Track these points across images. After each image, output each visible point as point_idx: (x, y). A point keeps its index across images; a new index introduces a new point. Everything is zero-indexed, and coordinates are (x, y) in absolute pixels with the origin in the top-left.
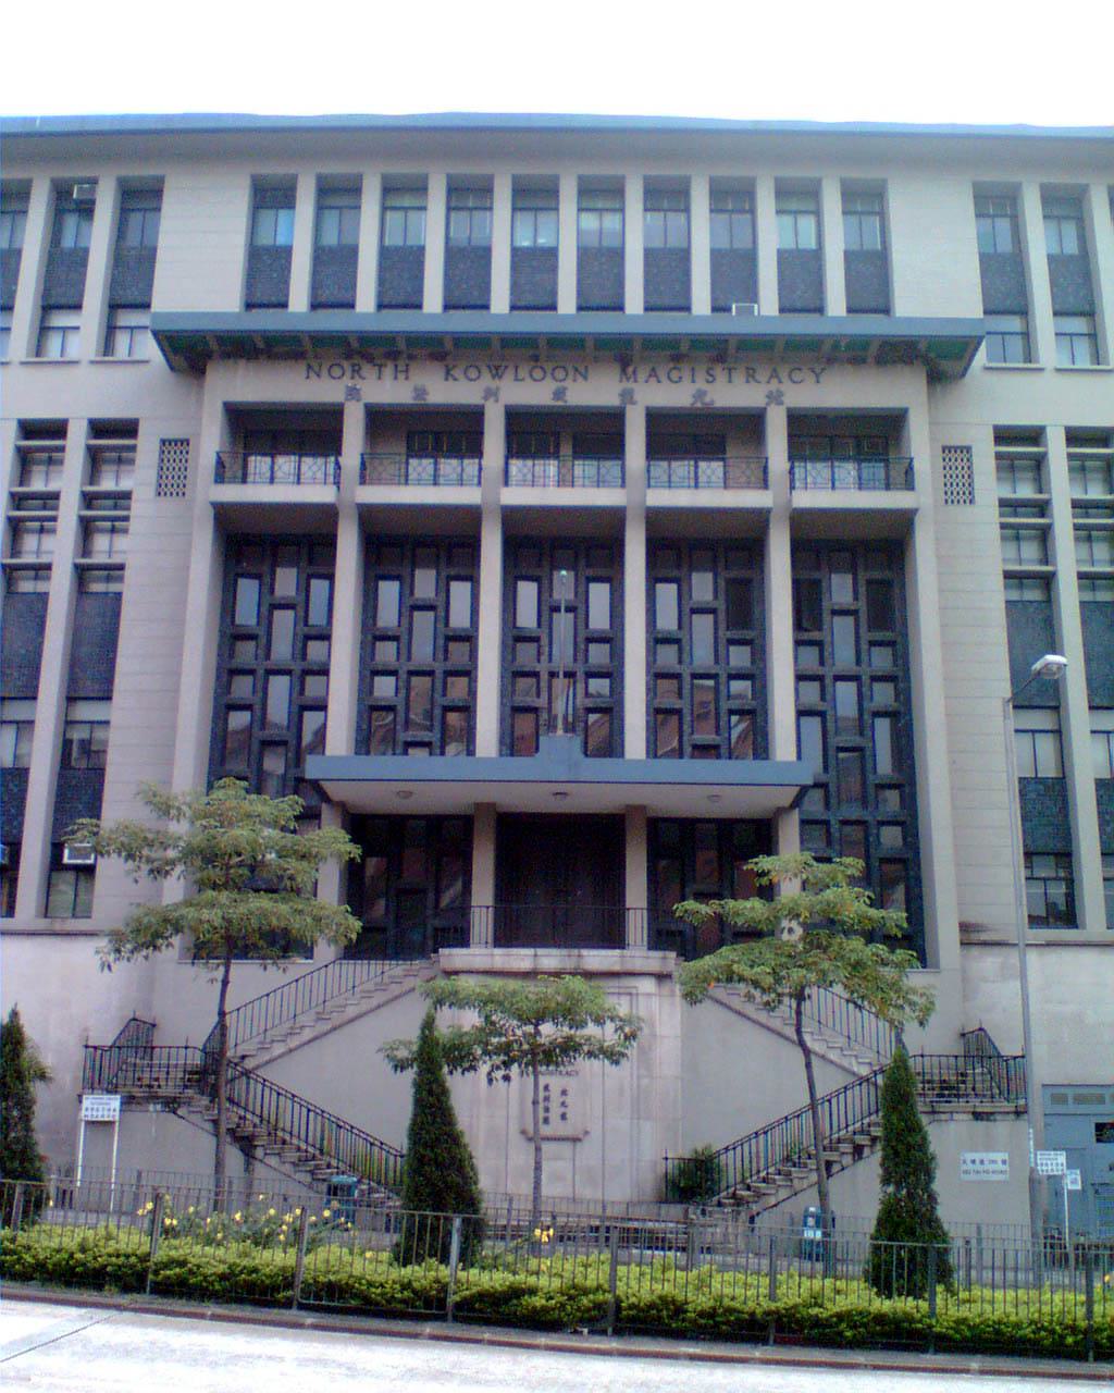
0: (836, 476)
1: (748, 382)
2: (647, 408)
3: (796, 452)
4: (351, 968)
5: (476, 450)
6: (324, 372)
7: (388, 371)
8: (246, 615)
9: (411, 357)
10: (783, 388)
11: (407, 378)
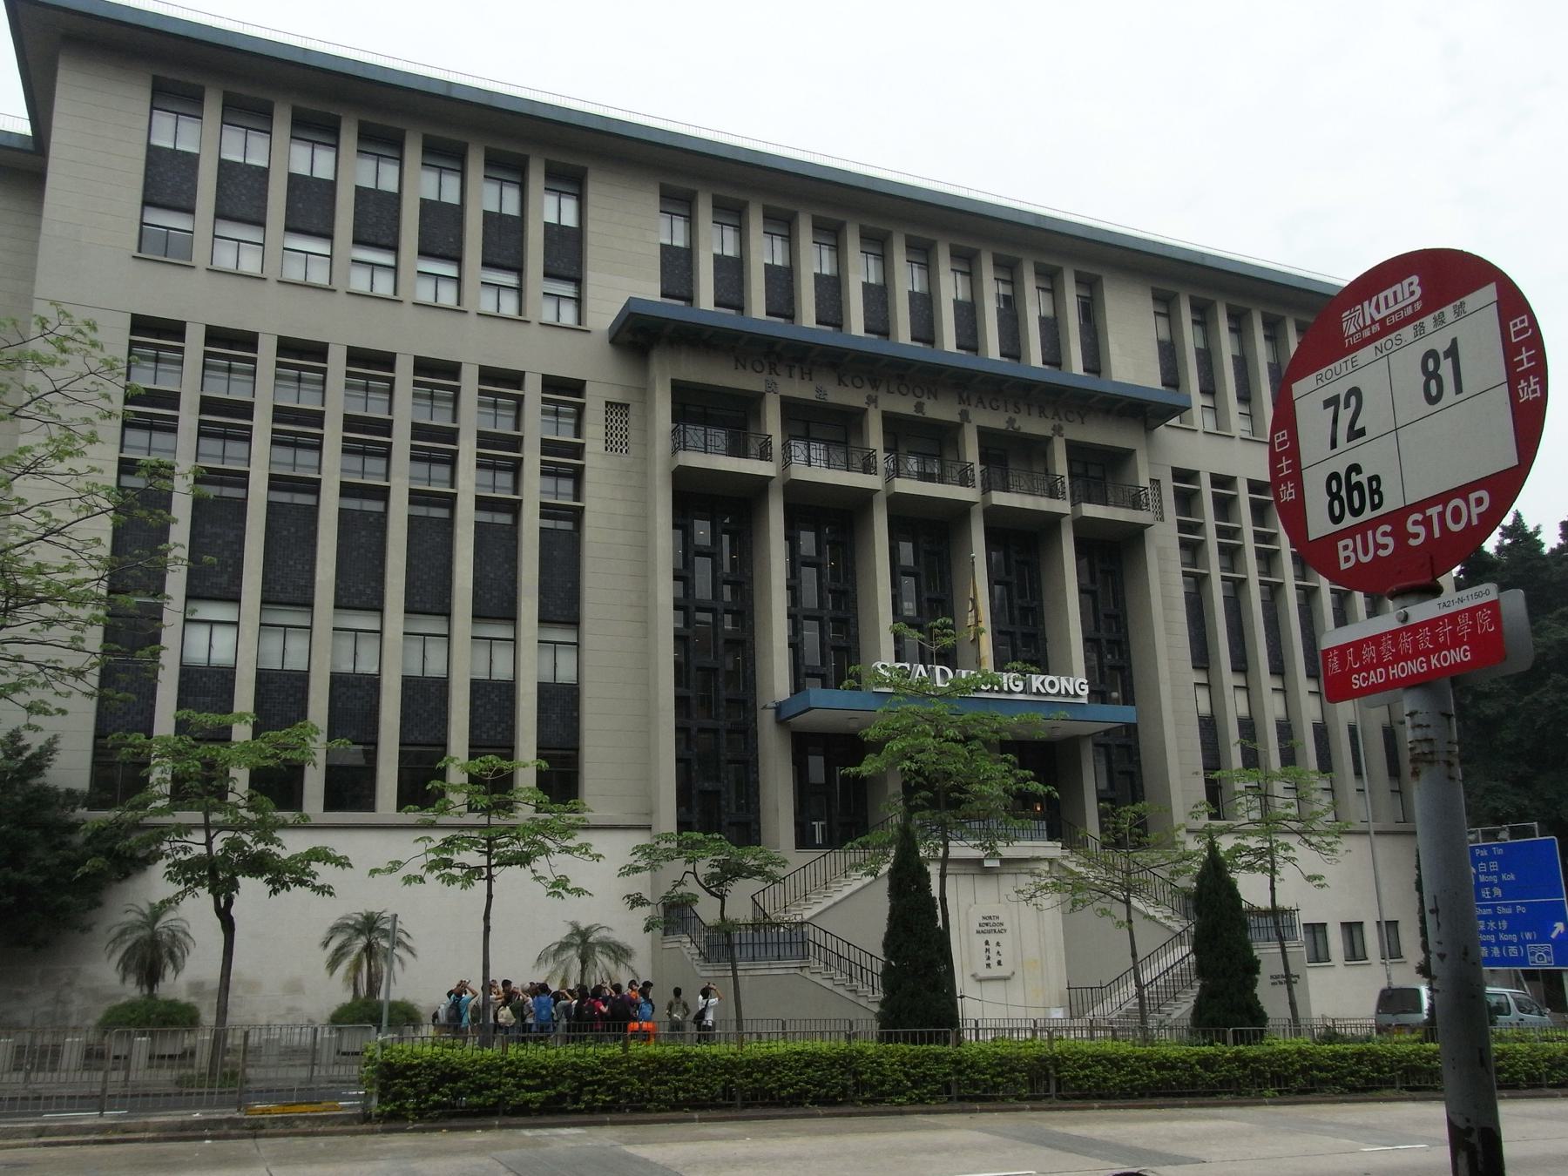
2: (978, 427)
3: (789, 435)
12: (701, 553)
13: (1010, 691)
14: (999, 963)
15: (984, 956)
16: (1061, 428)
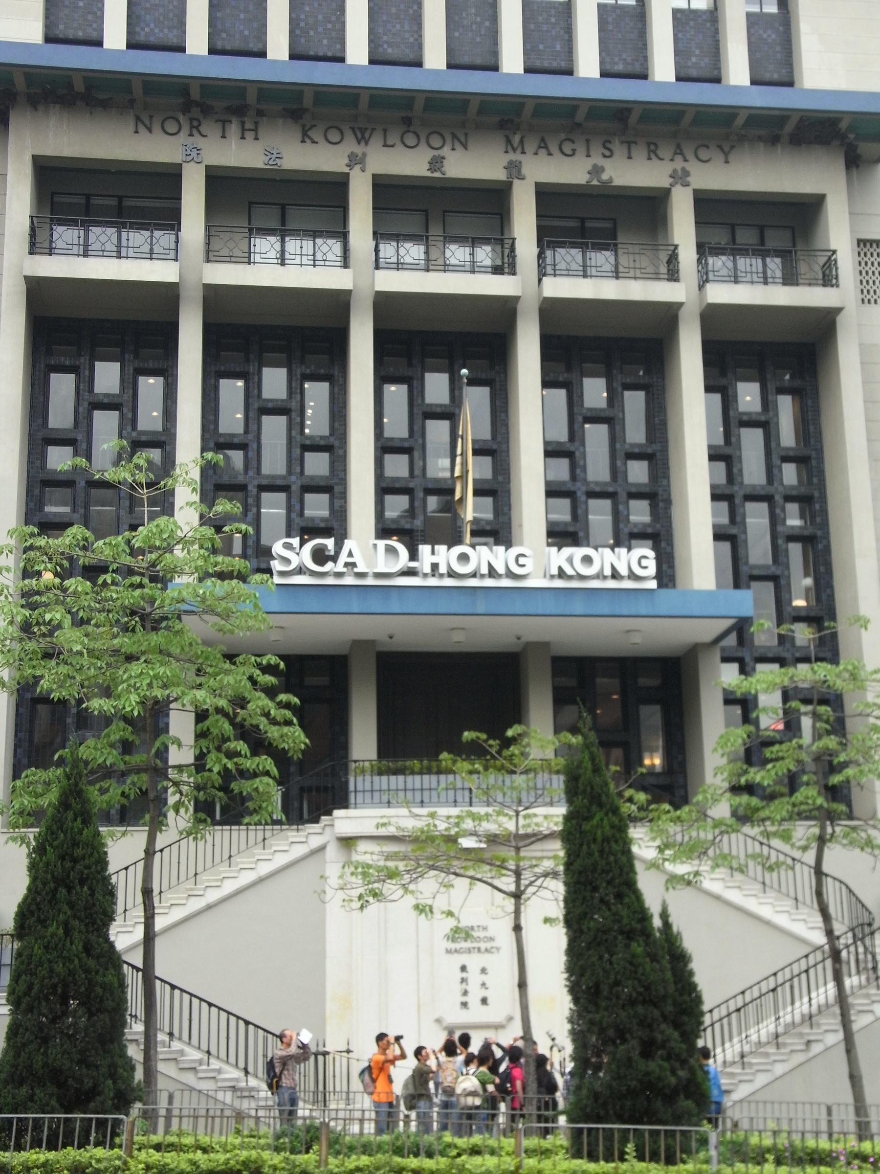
0: (124, 243)
1: (649, 159)
2: (537, 185)
3: (548, 237)
4: (226, 834)
5: (171, 219)
6: (156, 127)
7: (234, 129)
8: (61, 416)
9: (260, 113)
10: (688, 166)
11: (256, 139)
12: (595, 418)
13: (632, 576)
14: (484, 1001)
15: (459, 988)
16: (686, 173)
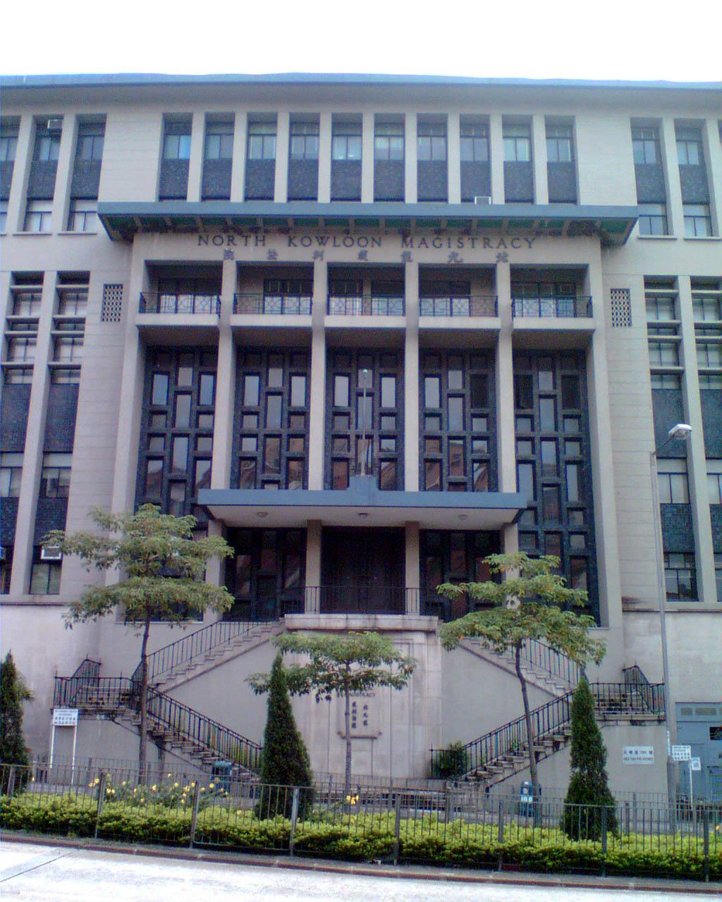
0: (542, 308)
1: (484, 247)
2: (420, 264)
3: (516, 293)
4: (228, 627)
5: (308, 292)
6: (210, 241)
7: (252, 240)
8: (160, 398)
9: (266, 231)
10: (507, 251)
11: (264, 245)
